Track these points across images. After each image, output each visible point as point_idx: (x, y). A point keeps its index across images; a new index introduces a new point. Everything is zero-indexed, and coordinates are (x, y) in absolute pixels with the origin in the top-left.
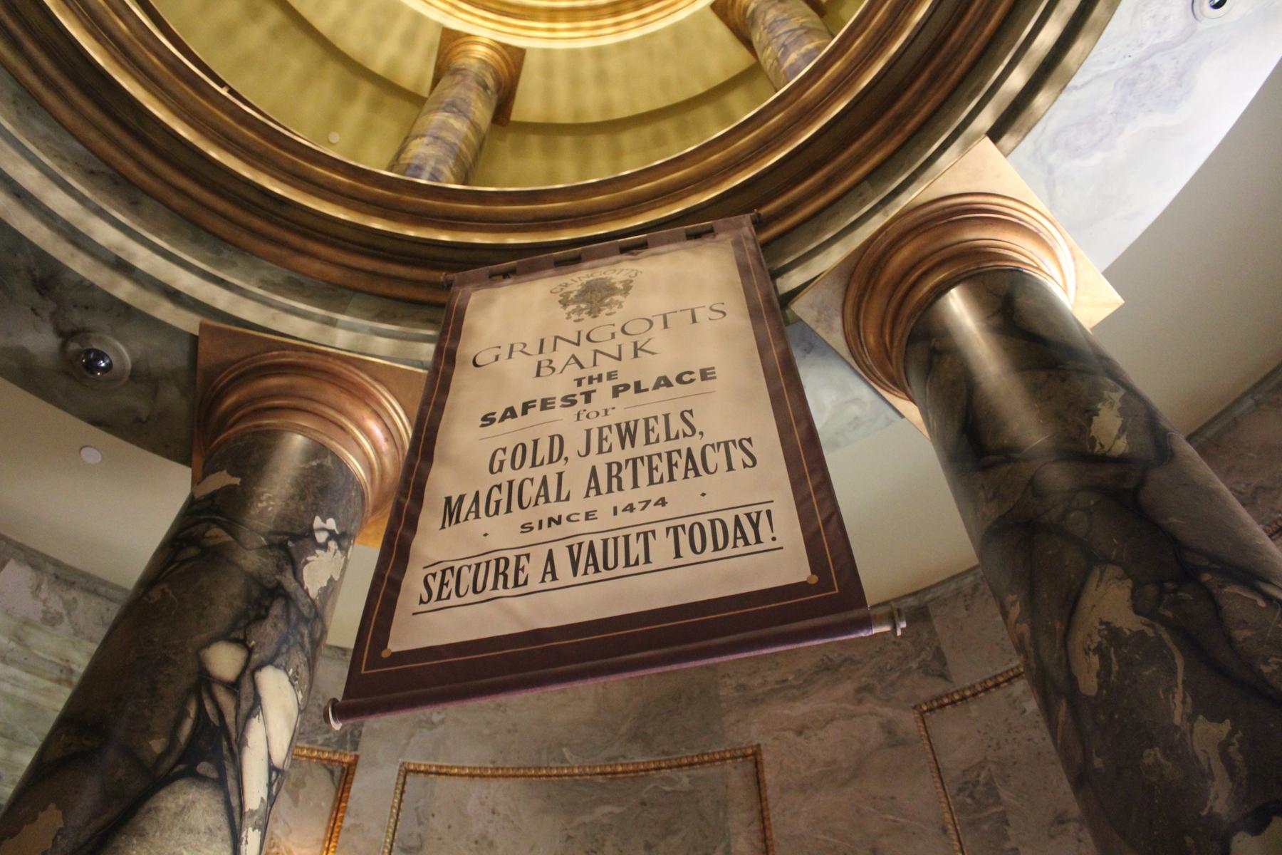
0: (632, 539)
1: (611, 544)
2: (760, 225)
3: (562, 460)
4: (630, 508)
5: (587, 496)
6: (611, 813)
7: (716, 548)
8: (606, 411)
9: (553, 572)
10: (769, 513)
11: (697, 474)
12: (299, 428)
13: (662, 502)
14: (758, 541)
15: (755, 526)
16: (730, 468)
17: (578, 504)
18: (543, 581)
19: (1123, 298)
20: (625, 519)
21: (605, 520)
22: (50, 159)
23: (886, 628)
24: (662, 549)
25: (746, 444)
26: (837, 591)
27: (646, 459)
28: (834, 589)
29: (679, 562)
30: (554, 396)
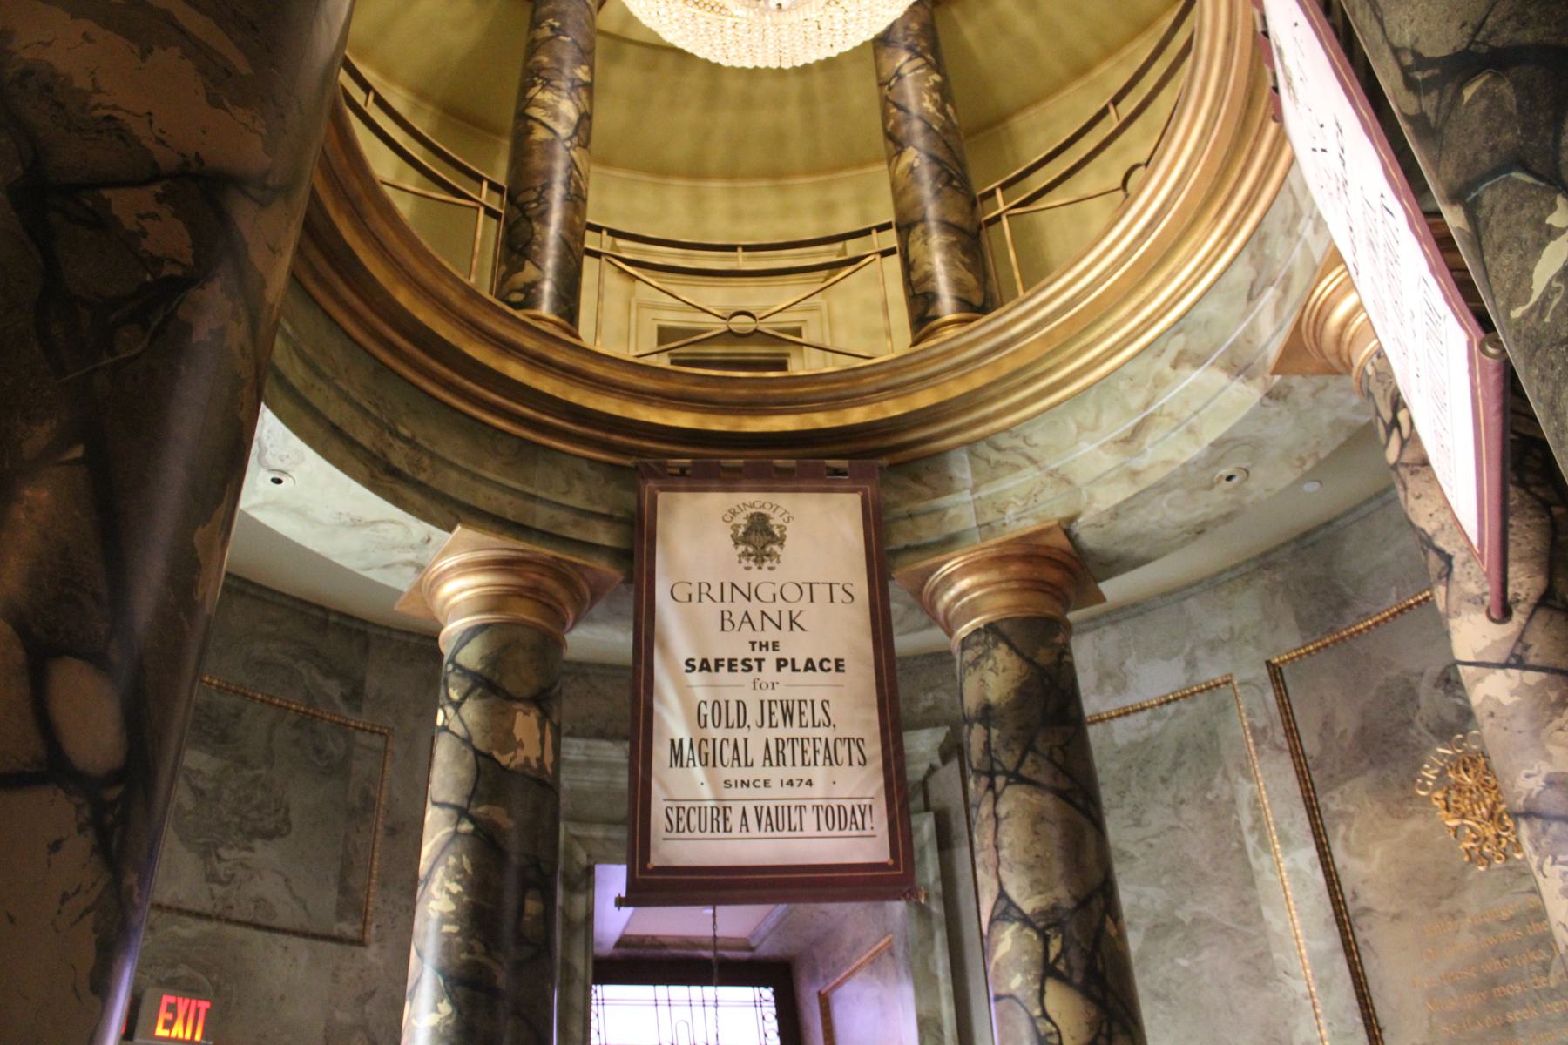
0: (793, 809)
1: (780, 810)
2: (782, 366)
3: (746, 727)
4: (791, 783)
5: (764, 765)
6: (183, 927)
7: (840, 828)
8: (773, 684)
9: (746, 825)
10: (871, 806)
11: (831, 764)
12: (252, 591)
13: (810, 783)
14: (864, 828)
15: (863, 815)
16: (851, 764)
17: (759, 772)
18: (741, 831)
19: (1098, 588)
20: (788, 792)
21: (776, 791)
22: (557, 232)
23: (116, 812)
24: (810, 818)
25: (860, 742)
26: (902, 872)
27: (811, 741)
28: (899, 869)
29: (819, 834)
30: (763, 669)
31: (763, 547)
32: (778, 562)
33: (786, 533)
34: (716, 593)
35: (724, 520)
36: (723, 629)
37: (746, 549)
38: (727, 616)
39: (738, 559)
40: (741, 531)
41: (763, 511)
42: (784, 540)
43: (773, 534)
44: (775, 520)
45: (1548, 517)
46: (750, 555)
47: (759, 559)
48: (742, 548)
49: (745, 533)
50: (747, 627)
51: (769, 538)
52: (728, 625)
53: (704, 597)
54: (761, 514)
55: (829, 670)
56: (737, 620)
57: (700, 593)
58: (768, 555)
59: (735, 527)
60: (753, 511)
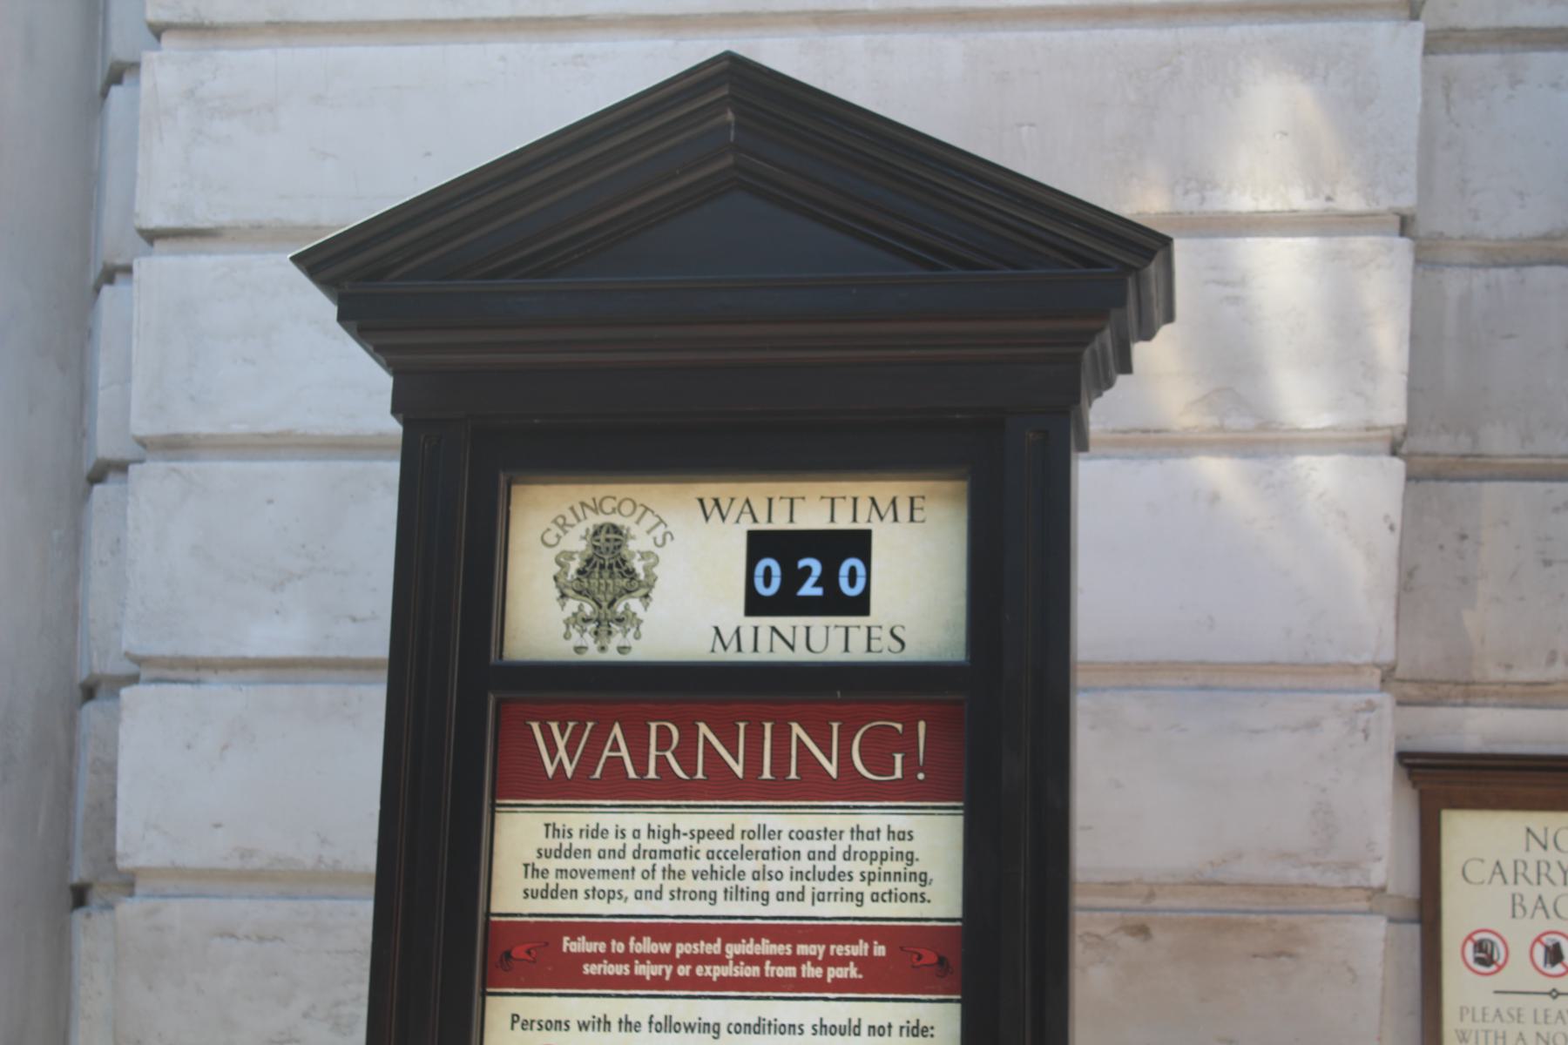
31: (611, 604)
32: (637, 637)
33: (656, 570)
34: (1532, 874)
35: (544, 543)
36: (1514, 916)
37: (580, 608)
38: (1518, 899)
39: (563, 628)
40: (575, 565)
41: (616, 519)
42: (650, 587)
43: (631, 573)
44: (638, 543)
45: (1497, 674)
46: (586, 620)
47: (604, 628)
48: (572, 605)
49: (581, 572)
50: (1540, 913)
51: (624, 583)
52: (1519, 911)
53: (1520, 878)
54: (615, 529)
55: (773, 839)
56: (1530, 903)
57: (1516, 874)
58: (620, 621)
59: (562, 560)
60: (601, 519)
